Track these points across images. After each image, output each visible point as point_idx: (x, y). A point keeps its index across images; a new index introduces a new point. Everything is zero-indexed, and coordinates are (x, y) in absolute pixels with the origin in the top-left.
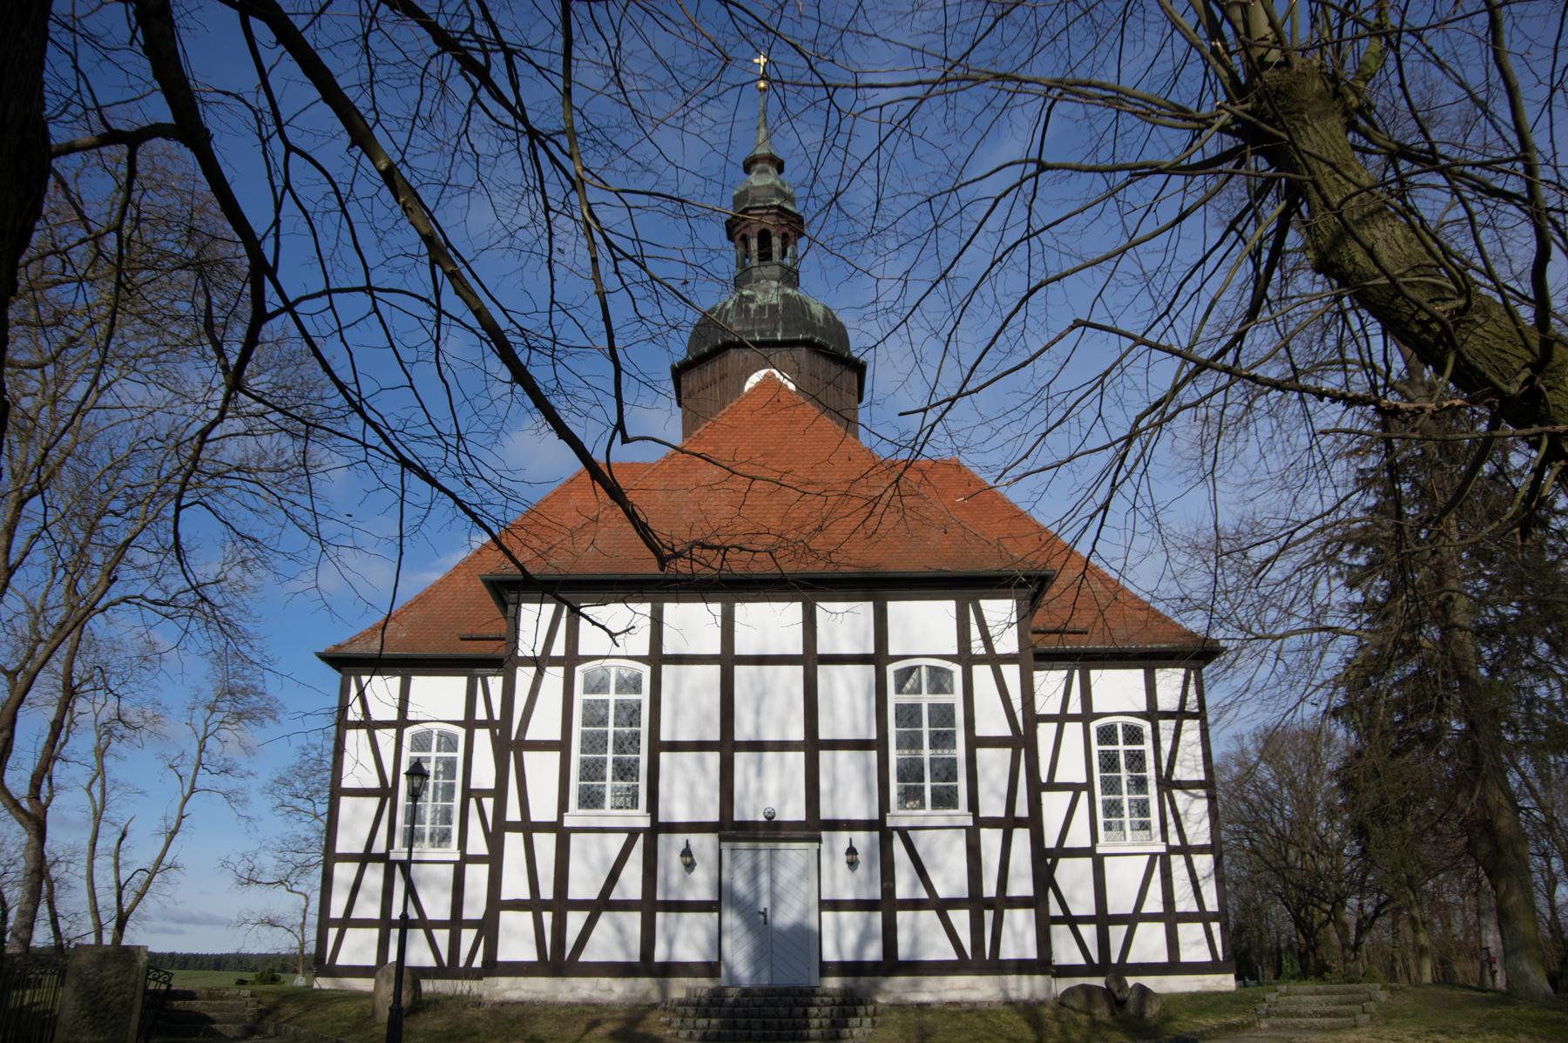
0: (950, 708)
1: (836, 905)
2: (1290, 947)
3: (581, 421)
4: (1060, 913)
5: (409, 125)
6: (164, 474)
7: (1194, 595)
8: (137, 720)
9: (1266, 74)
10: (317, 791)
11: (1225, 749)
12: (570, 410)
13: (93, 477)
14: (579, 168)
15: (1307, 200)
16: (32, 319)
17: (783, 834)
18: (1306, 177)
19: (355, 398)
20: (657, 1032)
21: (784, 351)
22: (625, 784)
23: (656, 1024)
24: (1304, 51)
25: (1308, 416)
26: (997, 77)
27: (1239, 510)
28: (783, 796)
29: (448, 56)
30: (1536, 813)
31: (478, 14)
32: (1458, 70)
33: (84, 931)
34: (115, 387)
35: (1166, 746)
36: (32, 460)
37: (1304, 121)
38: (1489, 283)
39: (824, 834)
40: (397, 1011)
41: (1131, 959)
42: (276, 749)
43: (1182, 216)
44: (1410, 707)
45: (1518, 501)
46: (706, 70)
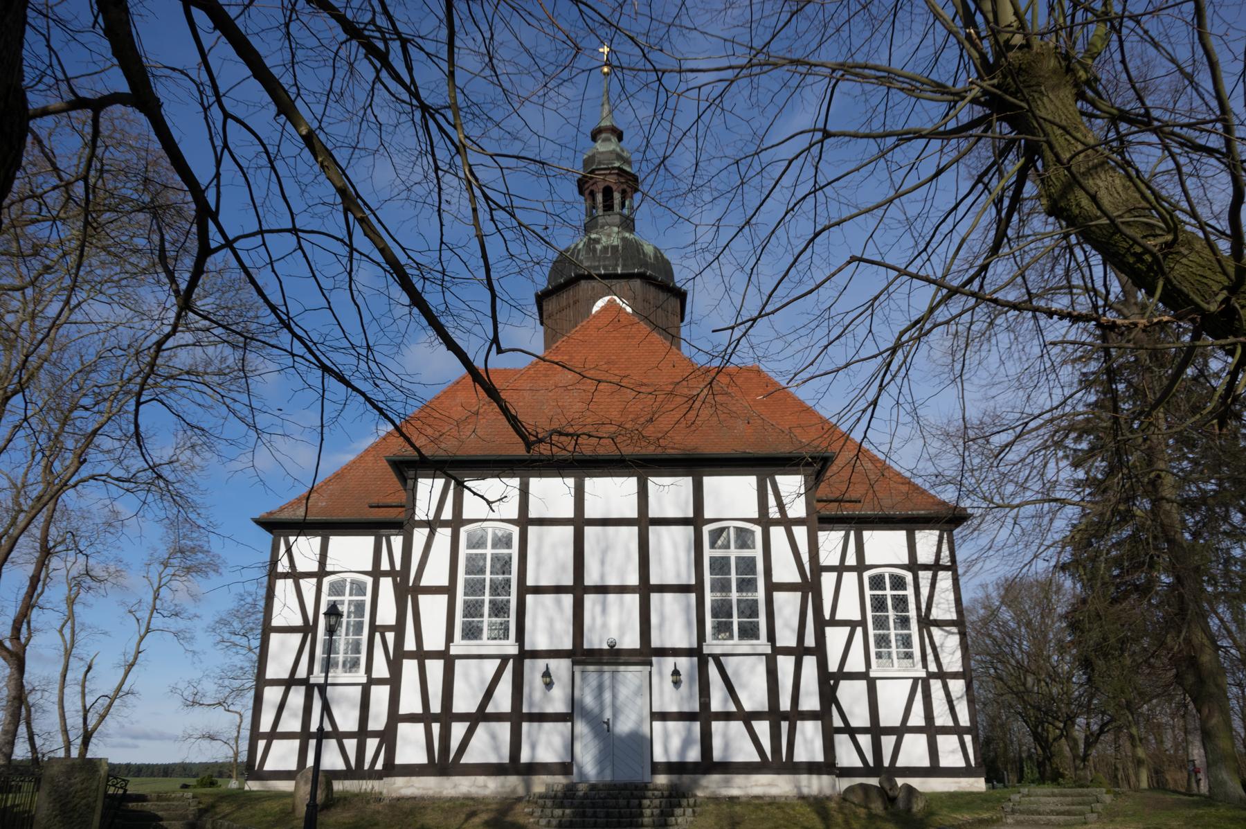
0: (752, 560)
1: (664, 716)
2: (1030, 757)
3: (465, 336)
4: (842, 725)
5: (324, 99)
6: (126, 376)
7: (946, 473)
8: (104, 575)
9: (1010, 54)
10: (252, 629)
11: (973, 595)
12: (456, 328)
13: (65, 379)
14: (461, 136)
15: (1042, 157)
16: (14, 250)
17: (623, 659)
18: (1042, 138)
19: (285, 317)
20: (522, 820)
21: (623, 282)
22: (499, 620)
23: (521, 814)
24: (1042, 35)
25: (1040, 331)
26: (792, 62)
27: (983, 406)
28: (622, 629)
29: (355, 43)
30: (1233, 651)
31: (378, 9)
32: (1169, 49)
33: (55, 747)
34: (84, 306)
35: (925, 592)
36: (15, 365)
37: (1041, 92)
38: (1193, 221)
39: (654, 659)
40: (313, 807)
41: (899, 764)
42: (218, 596)
43: (939, 172)
44: (1126, 564)
45: (1216, 398)
46: (561, 58)
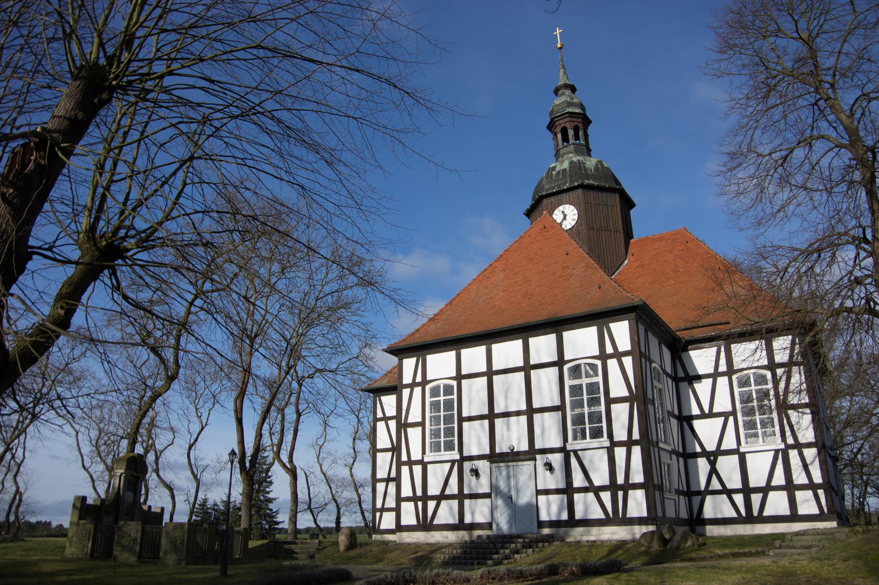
1: (547, 492)
4: (720, 488)
